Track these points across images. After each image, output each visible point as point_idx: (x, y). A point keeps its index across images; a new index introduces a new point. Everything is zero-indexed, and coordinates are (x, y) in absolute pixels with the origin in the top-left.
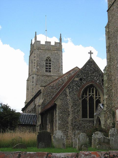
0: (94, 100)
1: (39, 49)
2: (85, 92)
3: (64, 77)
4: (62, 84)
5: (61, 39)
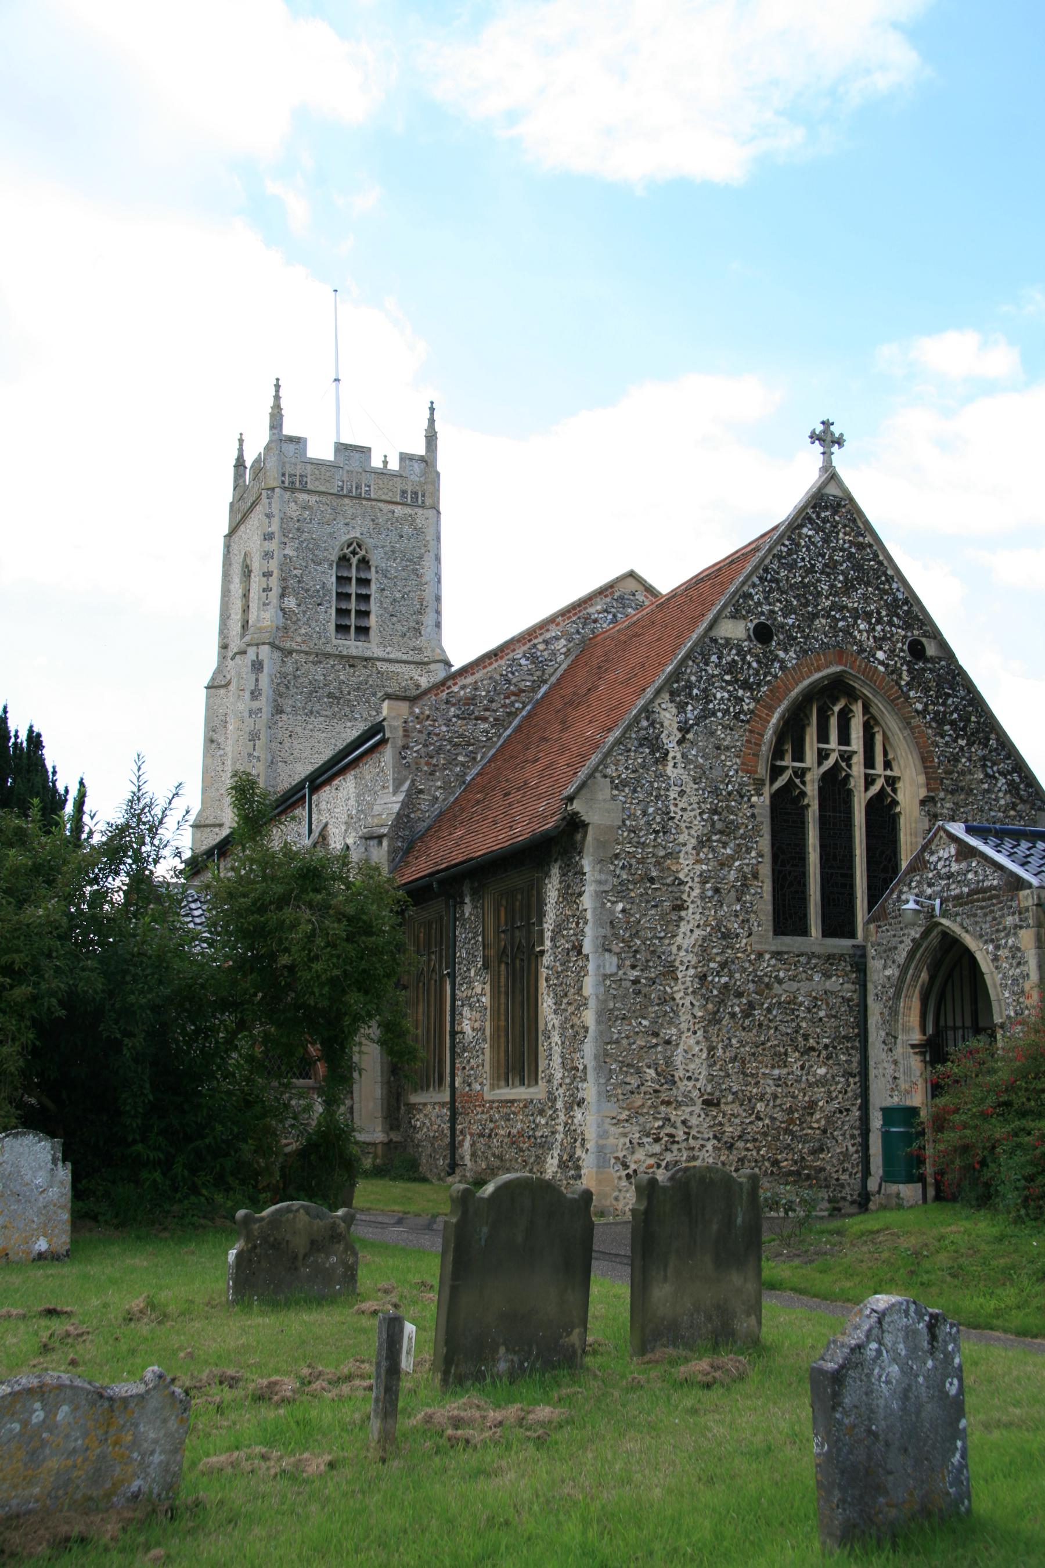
0: (849, 793)
1: (294, 485)
2: (791, 733)
3: (546, 642)
4: (534, 690)
5: (431, 438)
